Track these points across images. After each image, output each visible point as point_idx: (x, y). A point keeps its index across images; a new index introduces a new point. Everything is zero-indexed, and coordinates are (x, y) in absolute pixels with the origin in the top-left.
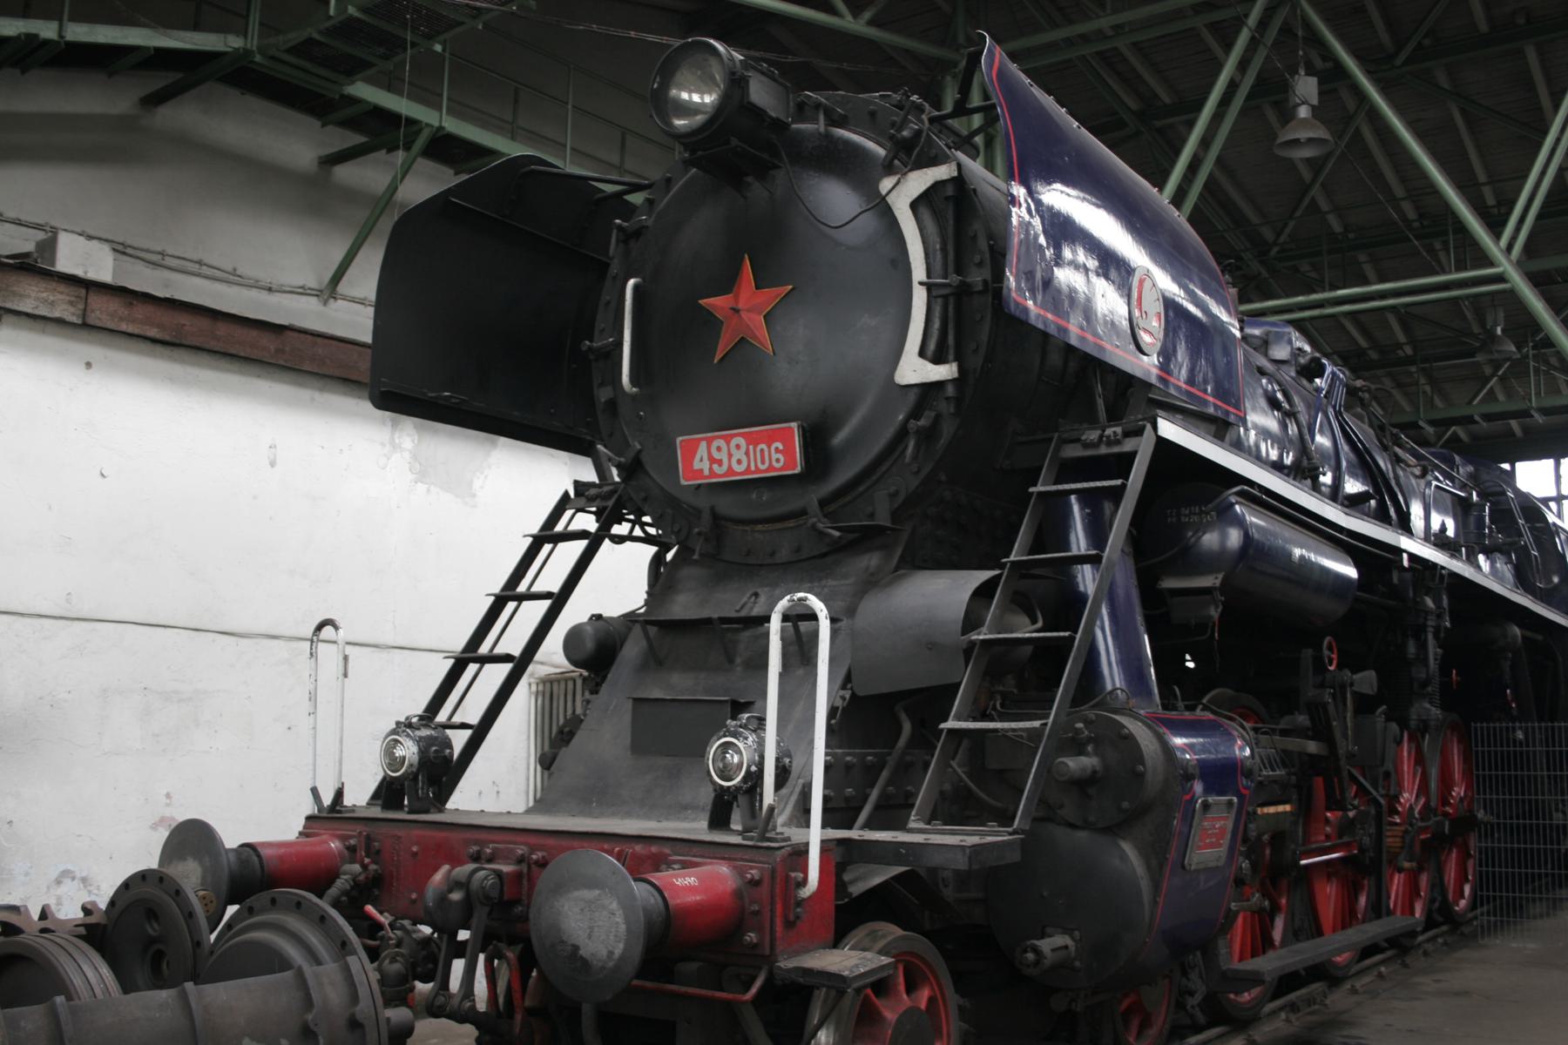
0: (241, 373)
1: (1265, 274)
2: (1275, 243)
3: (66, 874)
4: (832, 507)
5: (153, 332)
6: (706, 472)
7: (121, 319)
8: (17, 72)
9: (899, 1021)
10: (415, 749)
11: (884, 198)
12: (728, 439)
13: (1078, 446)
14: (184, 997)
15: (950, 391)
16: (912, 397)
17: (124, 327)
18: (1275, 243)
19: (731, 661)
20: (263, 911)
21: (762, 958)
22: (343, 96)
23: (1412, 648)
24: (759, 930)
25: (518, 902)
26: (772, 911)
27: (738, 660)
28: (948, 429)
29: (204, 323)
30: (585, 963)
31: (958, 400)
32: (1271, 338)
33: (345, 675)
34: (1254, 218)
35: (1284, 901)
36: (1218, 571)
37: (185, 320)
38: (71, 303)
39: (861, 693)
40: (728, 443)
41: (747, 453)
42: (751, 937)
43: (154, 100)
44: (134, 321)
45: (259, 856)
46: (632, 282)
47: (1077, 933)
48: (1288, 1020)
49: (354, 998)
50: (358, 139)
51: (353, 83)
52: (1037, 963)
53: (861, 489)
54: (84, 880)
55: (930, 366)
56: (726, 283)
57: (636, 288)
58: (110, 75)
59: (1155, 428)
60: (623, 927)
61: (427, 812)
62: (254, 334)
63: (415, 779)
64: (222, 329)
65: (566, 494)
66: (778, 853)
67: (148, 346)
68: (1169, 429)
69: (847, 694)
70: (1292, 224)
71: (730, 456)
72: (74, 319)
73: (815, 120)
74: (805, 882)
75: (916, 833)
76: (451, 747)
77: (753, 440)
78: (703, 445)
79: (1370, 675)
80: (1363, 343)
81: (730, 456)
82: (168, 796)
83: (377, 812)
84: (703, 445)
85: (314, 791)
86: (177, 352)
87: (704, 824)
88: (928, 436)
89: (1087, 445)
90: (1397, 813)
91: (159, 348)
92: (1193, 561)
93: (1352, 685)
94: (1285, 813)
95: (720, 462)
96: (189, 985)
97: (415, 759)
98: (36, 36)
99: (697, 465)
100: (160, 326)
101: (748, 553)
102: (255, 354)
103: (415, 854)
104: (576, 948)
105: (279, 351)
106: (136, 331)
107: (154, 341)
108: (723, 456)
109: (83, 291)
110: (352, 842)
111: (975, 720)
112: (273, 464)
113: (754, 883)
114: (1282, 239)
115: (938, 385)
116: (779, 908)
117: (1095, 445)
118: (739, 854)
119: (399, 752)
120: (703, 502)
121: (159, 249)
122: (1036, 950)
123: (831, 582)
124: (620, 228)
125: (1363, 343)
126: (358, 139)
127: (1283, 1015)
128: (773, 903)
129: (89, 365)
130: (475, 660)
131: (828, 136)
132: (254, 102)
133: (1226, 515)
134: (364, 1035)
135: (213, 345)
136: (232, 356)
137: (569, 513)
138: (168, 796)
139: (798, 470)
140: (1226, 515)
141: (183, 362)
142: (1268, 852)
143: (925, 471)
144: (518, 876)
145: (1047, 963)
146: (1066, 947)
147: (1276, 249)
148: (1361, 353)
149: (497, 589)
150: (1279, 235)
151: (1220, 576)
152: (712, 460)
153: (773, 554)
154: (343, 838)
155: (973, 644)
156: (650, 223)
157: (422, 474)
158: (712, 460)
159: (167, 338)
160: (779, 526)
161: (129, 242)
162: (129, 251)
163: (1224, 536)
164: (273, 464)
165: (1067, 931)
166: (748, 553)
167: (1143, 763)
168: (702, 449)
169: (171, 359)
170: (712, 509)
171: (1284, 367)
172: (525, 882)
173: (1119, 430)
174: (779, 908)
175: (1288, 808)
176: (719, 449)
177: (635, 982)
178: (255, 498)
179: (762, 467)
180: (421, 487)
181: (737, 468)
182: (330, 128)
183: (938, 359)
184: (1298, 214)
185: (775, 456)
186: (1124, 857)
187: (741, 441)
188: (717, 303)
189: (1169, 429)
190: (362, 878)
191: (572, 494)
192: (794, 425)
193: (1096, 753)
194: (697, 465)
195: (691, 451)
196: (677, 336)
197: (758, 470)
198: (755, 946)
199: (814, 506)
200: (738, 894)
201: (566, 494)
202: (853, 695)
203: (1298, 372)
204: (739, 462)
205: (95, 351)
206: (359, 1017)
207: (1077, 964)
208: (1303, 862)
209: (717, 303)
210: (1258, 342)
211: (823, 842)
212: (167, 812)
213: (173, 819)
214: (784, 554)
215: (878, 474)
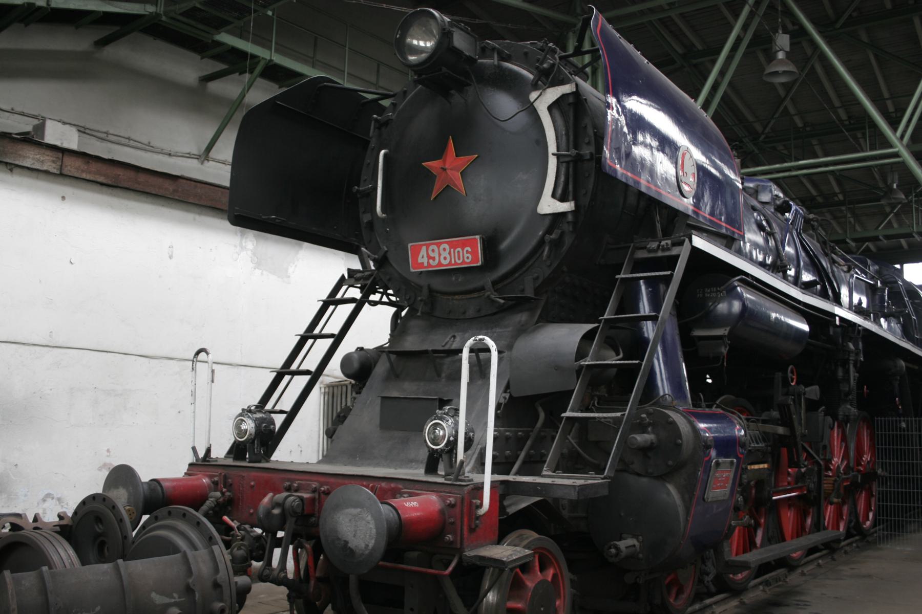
0: (152, 203)
1: (756, 151)
2: (763, 133)
3: (49, 496)
4: (500, 286)
5: (101, 179)
6: (426, 264)
7: (83, 171)
8: (23, 25)
10: (253, 425)
12: (438, 245)
13: (645, 251)
14: (117, 568)
16: (547, 222)
17: (84, 176)
18: (763, 133)
19: (439, 375)
20: (164, 518)
21: (455, 549)
22: (214, 41)
23: (840, 373)
25: (312, 515)
26: (462, 522)
27: (443, 375)
28: (568, 241)
29: (131, 174)
30: (352, 551)
31: (575, 223)
32: (760, 189)
33: (213, 381)
34: (750, 118)
35: (762, 521)
37: (120, 172)
38: (53, 162)
39: (515, 395)
40: (439, 247)
41: (450, 253)
42: (449, 537)
43: (103, 43)
44: (90, 173)
45: (161, 486)
46: (383, 152)
48: (764, 591)
49: (216, 570)
51: (220, 33)
52: (617, 555)
53: (517, 275)
54: (59, 499)
55: (558, 203)
56: (439, 153)
57: (385, 155)
58: (77, 28)
59: (691, 241)
60: (374, 531)
61: (259, 462)
62: (160, 181)
64: (142, 177)
65: (343, 276)
68: (699, 242)
69: (507, 396)
70: (773, 122)
71: (440, 255)
72: (55, 171)
73: (492, 58)
74: (481, 505)
76: (274, 424)
77: (453, 246)
78: (424, 248)
79: (816, 388)
80: (814, 193)
81: (440, 255)
82: (108, 451)
83: (230, 462)
84: (424, 248)
85: (194, 449)
86: (116, 191)
87: (422, 471)
88: (557, 244)
89: (650, 251)
90: (831, 470)
91: (105, 189)
92: (712, 320)
93: (805, 394)
95: (434, 259)
96: (120, 561)
97: (253, 431)
98: (33, 4)
99: (420, 260)
103: (252, 487)
104: (346, 542)
105: (175, 191)
106: (92, 178)
107: (102, 184)
109: (61, 155)
110: (216, 479)
112: (171, 257)
113: (451, 506)
114: (767, 130)
115: (563, 214)
116: (466, 520)
118: (443, 488)
119: (244, 427)
120: (423, 282)
121: (105, 130)
123: (498, 330)
124: (376, 120)
125: (814, 193)
127: (761, 587)
128: (462, 517)
129: (63, 198)
131: (499, 67)
133: (732, 293)
134: (222, 592)
135: (136, 187)
137: (344, 288)
139: (479, 264)
140: (732, 293)
141: (118, 196)
142: (754, 491)
143: (555, 265)
144: (313, 500)
145: (623, 555)
146: (634, 546)
147: (763, 137)
148: (813, 199)
149: (302, 332)
150: (765, 128)
151: (728, 329)
153: (464, 313)
154: (211, 477)
155: (581, 367)
156: (394, 117)
158: (429, 257)
159: (110, 183)
160: (468, 296)
161: (87, 126)
162: (87, 131)
163: (730, 306)
164: (171, 257)
165: (635, 536)
167: (681, 439)
168: (423, 251)
169: (111, 195)
170: (429, 287)
171: (767, 206)
172: (317, 504)
173: (669, 242)
175: (766, 466)
176: (433, 251)
177: (381, 563)
178: (160, 277)
180: (258, 272)
182: (206, 60)
183: (563, 199)
184: (777, 116)
185: (466, 255)
187: (447, 246)
189: (699, 242)
190: (221, 500)
191: (346, 277)
192: (478, 237)
193: (653, 432)
194: (420, 260)
195: (417, 252)
196: (410, 184)
197: (456, 264)
198: (452, 542)
199: (489, 285)
200: (441, 512)
201: (343, 276)
202: (511, 396)
203: (775, 209)
204: (445, 258)
205: (68, 190)
206: (219, 581)
207: (641, 555)
210: (752, 191)
211: (492, 482)
212: (108, 460)
213: (111, 464)
214: (471, 313)
215: (524, 269)
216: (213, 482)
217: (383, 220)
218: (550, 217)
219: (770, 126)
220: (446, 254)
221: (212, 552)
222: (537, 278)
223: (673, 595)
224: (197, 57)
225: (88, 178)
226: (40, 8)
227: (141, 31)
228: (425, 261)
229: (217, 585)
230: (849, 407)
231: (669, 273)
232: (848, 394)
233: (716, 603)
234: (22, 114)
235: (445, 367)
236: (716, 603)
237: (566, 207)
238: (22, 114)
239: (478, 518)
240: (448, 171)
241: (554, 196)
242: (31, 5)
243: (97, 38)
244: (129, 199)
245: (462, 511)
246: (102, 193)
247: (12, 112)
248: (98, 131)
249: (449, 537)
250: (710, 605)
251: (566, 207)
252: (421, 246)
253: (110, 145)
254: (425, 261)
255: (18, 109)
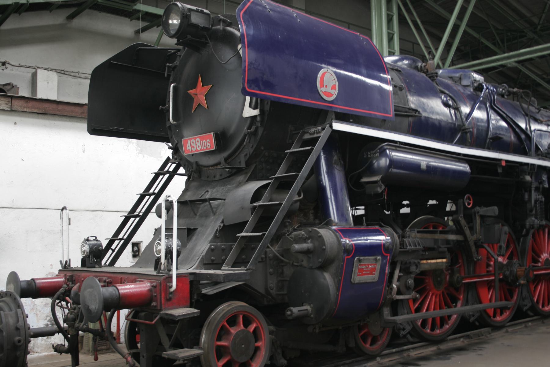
0: (70, 121)
2: (539, 24)
4: (229, 160)
5: (36, 111)
7: (24, 107)
8: (17, 14)
9: (236, 334)
10: (88, 247)
11: (238, 52)
13: (308, 134)
15: (258, 119)
16: (248, 122)
17: (25, 110)
18: (539, 24)
19: (196, 215)
23: (526, 196)
24: (156, 301)
27: (198, 214)
28: (260, 131)
29: (54, 106)
31: (262, 121)
32: (462, 77)
33: (69, 224)
34: (528, 15)
35: (462, 297)
36: (380, 174)
38: (6, 104)
39: (226, 224)
42: (154, 304)
43: (71, 17)
44: (29, 108)
45: (35, 282)
46: (172, 85)
47: (312, 305)
48: (463, 342)
49: (18, 321)
50: (146, 24)
52: (291, 315)
53: (237, 154)
56: (194, 86)
57: (174, 87)
59: (331, 126)
61: (94, 267)
62: (72, 108)
63: (89, 257)
64: (61, 107)
65: (168, 158)
66: (163, 277)
67: (36, 115)
69: (222, 225)
70: (544, 15)
71: (196, 145)
72: (8, 109)
73: (219, 25)
74: (171, 287)
75: (225, 270)
76: (102, 247)
77: (202, 139)
79: (496, 208)
81: (196, 145)
82: (51, 265)
85: (61, 261)
86: (46, 116)
87: (153, 269)
88: (255, 133)
90: (539, 262)
91: (40, 116)
92: (371, 171)
93: (478, 213)
94: (442, 262)
97: (88, 251)
98: (18, 3)
99: (188, 148)
100: (38, 108)
101: (208, 177)
102: (73, 114)
105: (82, 113)
106: (30, 111)
107: (38, 113)
108: (194, 145)
109: (10, 99)
111: (252, 232)
112: (84, 152)
113: (155, 287)
114: (541, 22)
116: (163, 295)
117: (314, 133)
118: (153, 277)
119: (84, 248)
120: (192, 160)
122: (291, 311)
123: (229, 186)
126: (146, 24)
127: (462, 339)
128: (161, 293)
129: (15, 123)
130: (133, 217)
131: (224, 30)
132: (103, 14)
133: (383, 153)
134: (20, 332)
135: (57, 113)
136: (66, 116)
138: (51, 265)
139: (214, 149)
140: (383, 153)
141: (49, 119)
142: (448, 277)
143: (255, 146)
146: (307, 310)
147: (539, 27)
150: (540, 19)
151: (381, 176)
152: (192, 147)
153: (214, 177)
154: (151, 283)
155: (255, 207)
157: (141, 151)
158: (192, 147)
159: (41, 112)
160: (216, 167)
164: (84, 152)
166: (208, 177)
167: (325, 245)
169: (44, 119)
170: (197, 162)
171: (469, 88)
174: (163, 295)
178: (78, 163)
179: (205, 148)
180: (141, 156)
181: (199, 149)
183: (255, 108)
185: (208, 144)
186: (325, 279)
187: (198, 139)
188: (191, 92)
189: (338, 126)
191: (171, 157)
192: (212, 133)
193: (311, 242)
194: (188, 148)
196: (184, 103)
197: (204, 149)
198: (155, 306)
199: (223, 161)
200: (150, 290)
201: (168, 158)
202: (224, 225)
203: (474, 90)
205: (17, 119)
206: (18, 326)
207: (312, 316)
208: (464, 281)
209: (191, 92)
210: (458, 79)
212: (52, 271)
213: (53, 273)
214: (218, 177)
216: (153, 286)
217: (174, 125)
218: (249, 119)
219: (543, 19)
220: (198, 144)
221: (16, 313)
222: (246, 155)
223: (369, 342)
224: (128, 20)
225: (28, 111)
226: (23, 5)
227: (90, 8)
228: (190, 148)
229: (17, 329)
230: (533, 218)
231: (309, 148)
232: (531, 211)
233: (413, 348)
234: (26, 67)
235: (200, 209)
236: (413, 348)
237: (256, 112)
238: (26, 67)
239: (171, 293)
240: (198, 95)
241: (250, 106)
242: (17, 4)
243: (67, 15)
244: (55, 120)
245: (161, 290)
246: (39, 118)
247: (19, 66)
248: (73, 72)
249: (154, 304)
250: (408, 350)
251: (256, 112)
252: (188, 140)
253: (79, 80)
254: (190, 148)
255: (23, 64)
